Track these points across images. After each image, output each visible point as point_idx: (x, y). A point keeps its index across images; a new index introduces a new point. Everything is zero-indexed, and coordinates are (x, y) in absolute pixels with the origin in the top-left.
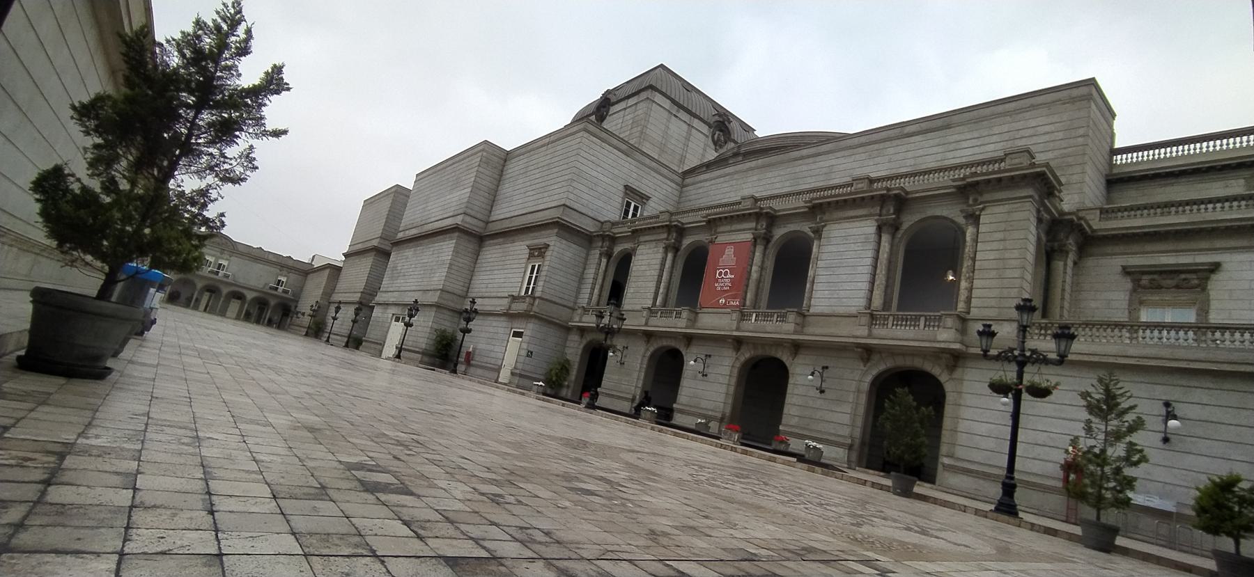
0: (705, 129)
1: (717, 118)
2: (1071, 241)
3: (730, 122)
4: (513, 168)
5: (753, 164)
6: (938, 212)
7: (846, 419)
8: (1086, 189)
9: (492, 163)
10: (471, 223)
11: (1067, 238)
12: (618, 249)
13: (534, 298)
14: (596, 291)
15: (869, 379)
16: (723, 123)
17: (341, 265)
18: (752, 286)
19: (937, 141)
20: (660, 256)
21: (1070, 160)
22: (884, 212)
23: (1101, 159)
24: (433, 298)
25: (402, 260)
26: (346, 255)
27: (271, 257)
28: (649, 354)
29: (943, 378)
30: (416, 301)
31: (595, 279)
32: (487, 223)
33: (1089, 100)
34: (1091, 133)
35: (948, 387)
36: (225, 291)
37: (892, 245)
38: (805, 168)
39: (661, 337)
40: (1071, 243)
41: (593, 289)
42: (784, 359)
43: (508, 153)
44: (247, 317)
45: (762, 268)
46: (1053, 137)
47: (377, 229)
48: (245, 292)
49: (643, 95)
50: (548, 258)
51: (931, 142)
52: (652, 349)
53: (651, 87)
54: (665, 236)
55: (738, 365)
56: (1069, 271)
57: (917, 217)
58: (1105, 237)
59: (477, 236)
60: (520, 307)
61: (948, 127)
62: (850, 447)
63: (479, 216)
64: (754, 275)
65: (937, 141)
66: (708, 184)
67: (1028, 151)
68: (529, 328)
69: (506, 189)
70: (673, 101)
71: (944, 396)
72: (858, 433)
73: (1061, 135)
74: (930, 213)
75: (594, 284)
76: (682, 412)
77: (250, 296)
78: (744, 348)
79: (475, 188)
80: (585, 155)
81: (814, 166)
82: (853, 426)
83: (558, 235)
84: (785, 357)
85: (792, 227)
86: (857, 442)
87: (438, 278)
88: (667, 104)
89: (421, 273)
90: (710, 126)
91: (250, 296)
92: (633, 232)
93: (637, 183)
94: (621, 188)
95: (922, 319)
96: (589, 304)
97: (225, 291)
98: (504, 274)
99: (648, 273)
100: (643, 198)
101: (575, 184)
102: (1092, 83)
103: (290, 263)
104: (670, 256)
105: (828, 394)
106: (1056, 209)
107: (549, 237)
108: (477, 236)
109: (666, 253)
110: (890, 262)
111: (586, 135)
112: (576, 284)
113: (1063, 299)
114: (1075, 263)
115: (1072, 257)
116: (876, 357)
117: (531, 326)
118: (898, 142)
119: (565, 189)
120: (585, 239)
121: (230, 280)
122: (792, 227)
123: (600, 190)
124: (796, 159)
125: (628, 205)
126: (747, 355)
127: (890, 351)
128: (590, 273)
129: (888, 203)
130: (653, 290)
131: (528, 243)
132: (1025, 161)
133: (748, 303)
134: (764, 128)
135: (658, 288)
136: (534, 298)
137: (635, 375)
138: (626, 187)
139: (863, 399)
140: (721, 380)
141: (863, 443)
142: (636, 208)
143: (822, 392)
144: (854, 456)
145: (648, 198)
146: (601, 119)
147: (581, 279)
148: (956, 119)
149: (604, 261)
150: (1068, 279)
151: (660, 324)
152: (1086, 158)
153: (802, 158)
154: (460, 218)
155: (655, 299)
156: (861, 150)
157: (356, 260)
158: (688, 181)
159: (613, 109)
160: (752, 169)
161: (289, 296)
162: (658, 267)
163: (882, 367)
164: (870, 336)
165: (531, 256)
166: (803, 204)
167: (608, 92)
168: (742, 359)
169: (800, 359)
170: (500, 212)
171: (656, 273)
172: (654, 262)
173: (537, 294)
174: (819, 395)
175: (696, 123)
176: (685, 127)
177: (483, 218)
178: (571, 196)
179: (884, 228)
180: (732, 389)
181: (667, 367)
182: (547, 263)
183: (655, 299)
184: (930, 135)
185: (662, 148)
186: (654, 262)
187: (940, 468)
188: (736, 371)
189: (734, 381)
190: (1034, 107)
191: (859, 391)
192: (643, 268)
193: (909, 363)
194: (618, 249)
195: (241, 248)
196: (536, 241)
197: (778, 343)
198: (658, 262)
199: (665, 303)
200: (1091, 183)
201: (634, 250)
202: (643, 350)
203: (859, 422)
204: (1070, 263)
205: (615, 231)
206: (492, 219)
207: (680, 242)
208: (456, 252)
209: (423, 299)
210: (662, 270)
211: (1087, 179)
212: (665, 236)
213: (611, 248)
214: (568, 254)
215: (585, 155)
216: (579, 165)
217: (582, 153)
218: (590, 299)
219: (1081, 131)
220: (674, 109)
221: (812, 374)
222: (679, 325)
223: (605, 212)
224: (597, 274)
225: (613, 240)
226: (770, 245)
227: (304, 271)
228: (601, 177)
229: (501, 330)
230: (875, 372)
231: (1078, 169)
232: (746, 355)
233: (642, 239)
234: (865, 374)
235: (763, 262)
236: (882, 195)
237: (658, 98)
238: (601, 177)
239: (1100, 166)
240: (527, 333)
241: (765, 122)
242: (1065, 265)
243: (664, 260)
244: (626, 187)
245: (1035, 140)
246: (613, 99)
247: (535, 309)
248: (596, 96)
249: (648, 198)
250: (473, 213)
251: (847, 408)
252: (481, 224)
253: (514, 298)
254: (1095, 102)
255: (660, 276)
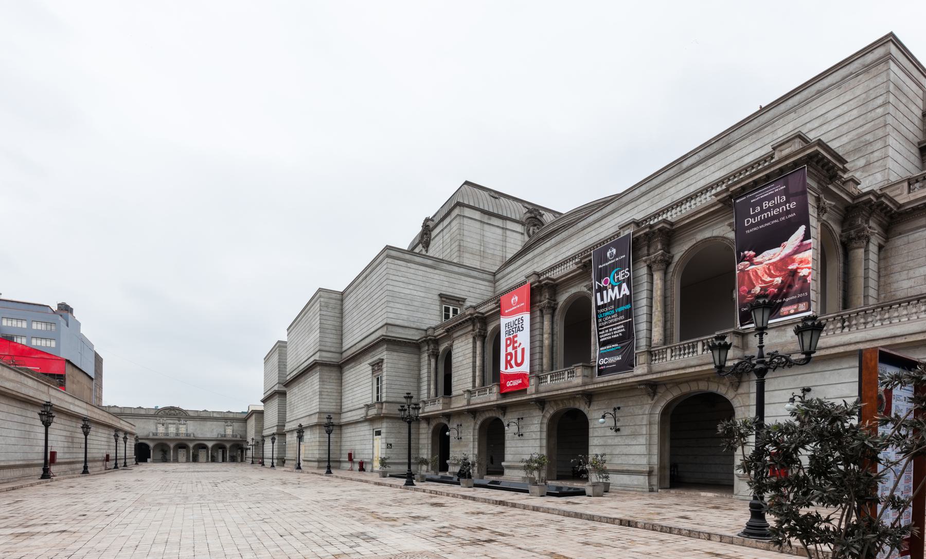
0: (519, 228)
1: (528, 215)
2: (872, 224)
3: (542, 215)
4: (349, 303)
5: (548, 244)
6: (707, 234)
7: (643, 449)
8: (890, 164)
9: (332, 305)
10: (328, 357)
11: (867, 222)
12: (442, 348)
13: (382, 403)
14: (432, 386)
15: (658, 410)
16: (535, 218)
17: (262, 408)
18: (546, 352)
19: (718, 165)
20: (471, 346)
21: (868, 137)
22: (652, 250)
23: (912, 128)
24: (315, 420)
25: (295, 395)
26: (264, 401)
27: (215, 415)
28: (477, 427)
29: (730, 395)
30: (300, 426)
31: (429, 377)
32: (342, 353)
33: (886, 61)
34: (892, 99)
35: (736, 403)
36: (191, 445)
37: (665, 281)
38: (593, 233)
39: (483, 411)
40: (873, 227)
41: (429, 385)
42: (582, 408)
43: (342, 293)
44: (214, 460)
45: (552, 334)
46: (846, 118)
47: (275, 379)
48: (206, 443)
49: (456, 211)
50: (385, 370)
51: (712, 169)
52: (479, 422)
53: (459, 204)
54: (471, 328)
55: (546, 421)
56: (873, 256)
57: (686, 247)
58: (914, 209)
59: (335, 366)
60: (373, 412)
61: (728, 146)
62: (650, 473)
63: (333, 349)
64: (546, 342)
65: (718, 165)
66: (515, 273)
67: (800, 136)
68: (384, 427)
69: (348, 322)
70: (483, 212)
71: (734, 413)
72: (655, 460)
73: (855, 113)
74: (700, 237)
75: (429, 381)
76: (509, 467)
77: (210, 445)
78: (547, 407)
79: (322, 330)
80: (394, 278)
81: (602, 230)
82: (650, 454)
83: (387, 350)
84: (583, 407)
85: (573, 290)
86: (656, 468)
87: (315, 406)
88: (477, 215)
89: (306, 403)
90: (523, 224)
91: (210, 445)
92: (448, 331)
93: (451, 290)
94: (437, 297)
95: (700, 345)
96: (428, 397)
97: (191, 445)
98: (359, 389)
99: (465, 362)
100: (460, 301)
101: (391, 305)
102: (891, 34)
103: (231, 416)
104: (479, 344)
105: (625, 431)
106: (848, 194)
107: (382, 353)
108: (335, 366)
109: (474, 343)
110: (665, 297)
111: (390, 260)
112: (416, 385)
113: (866, 287)
114: (880, 247)
115: (874, 242)
116: (661, 390)
117: (385, 425)
118: (679, 179)
119: (384, 311)
120: (414, 347)
121: (192, 437)
122: (573, 290)
123: (416, 304)
124: (584, 228)
125: (447, 310)
126: (552, 412)
127: (675, 382)
128: (424, 372)
129: (649, 241)
130: (471, 375)
131: (370, 361)
132: (797, 145)
133: (545, 367)
134: (564, 208)
135: (474, 372)
136: (382, 403)
137: (471, 445)
138: (441, 296)
139: (656, 429)
140: (534, 436)
141: (662, 468)
142: (455, 311)
143: (617, 430)
144: (655, 481)
145: (464, 300)
146: (427, 245)
147: (419, 379)
148: (736, 135)
149: (433, 361)
150: (873, 266)
151: (551, 385)
152: (889, 128)
153: (589, 225)
154: (318, 354)
155: (474, 381)
156: (643, 199)
157: (269, 403)
158: (498, 276)
159: (434, 234)
160: (547, 249)
161: (238, 438)
162: (471, 355)
163: (669, 397)
164: (650, 372)
165: (373, 371)
166: (575, 267)
167: (427, 220)
168: (548, 416)
169: (594, 406)
170: (348, 342)
171: (471, 360)
172: (467, 352)
173: (384, 399)
174: (615, 434)
175: (510, 225)
176: (499, 231)
177: (338, 350)
178: (391, 315)
179: (655, 267)
180: (544, 442)
181: (492, 436)
182: (385, 374)
183: (474, 381)
184: (710, 161)
185: (482, 255)
186: (467, 352)
187: (736, 478)
188: (545, 427)
189: (544, 435)
190: (820, 93)
191: (650, 424)
192: (461, 359)
193: (694, 388)
194: (442, 348)
195: (192, 414)
196: (374, 359)
197: (573, 396)
198: (471, 350)
199: (483, 383)
200: (900, 159)
201: (451, 346)
202: (473, 424)
203: (655, 450)
204: (873, 248)
205: (436, 334)
206: (344, 349)
207: (486, 330)
208: (322, 381)
209: (305, 423)
210: (474, 357)
211: (891, 152)
212: (471, 328)
213: (432, 347)
214: (401, 362)
215: (394, 278)
216: (390, 288)
217: (391, 272)
218: (429, 393)
219: (880, 101)
220: (485, 218)
221: (604, 417)
222: (492, 399)
223: (426, 321)
224: (429, 372)
225: (436, 342)
226: (671, 269)
227: (244, 419)
228: (415, 293)
229: (367, 432)
230: (663, 404)
231: (879, 145)
232: (550, 411)
233: (455, 335)
234: (654, 407)
235: (552, 329)
236: (646, 234)
237: (468, 212)
238: (415, 293)
239: (911, 137)
240: (383, 431)
241: (562, 201)
242: (867, 251)
243: (474, 347)
244: (441, 296)
245: (825, 128)
246: (431, 224)
247: (384, 411)
248: (419, 229)
249: (464, 300)
250: (327, 349)
251: (642, 440)
252: (337, 355)
253: (368, 407)
254: (896, 61)
255: (474, 362)
